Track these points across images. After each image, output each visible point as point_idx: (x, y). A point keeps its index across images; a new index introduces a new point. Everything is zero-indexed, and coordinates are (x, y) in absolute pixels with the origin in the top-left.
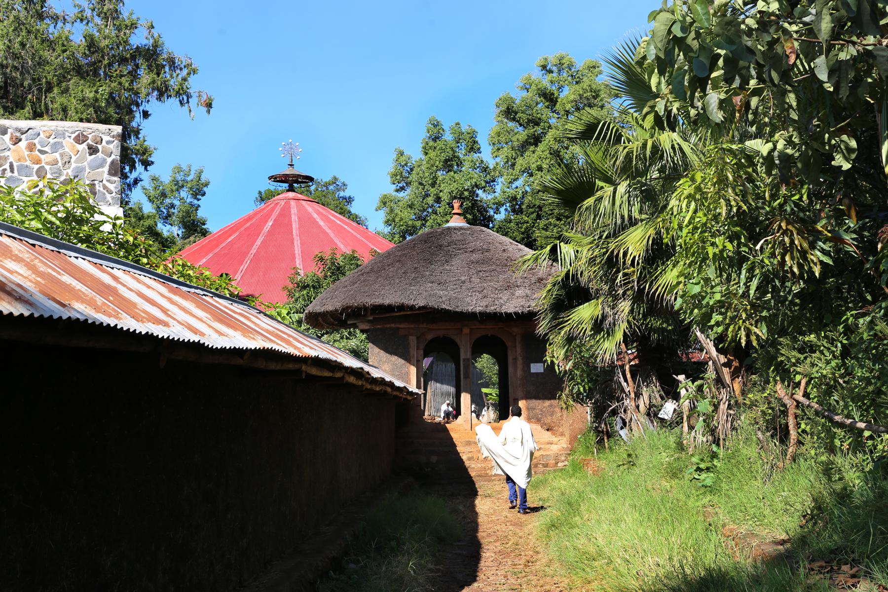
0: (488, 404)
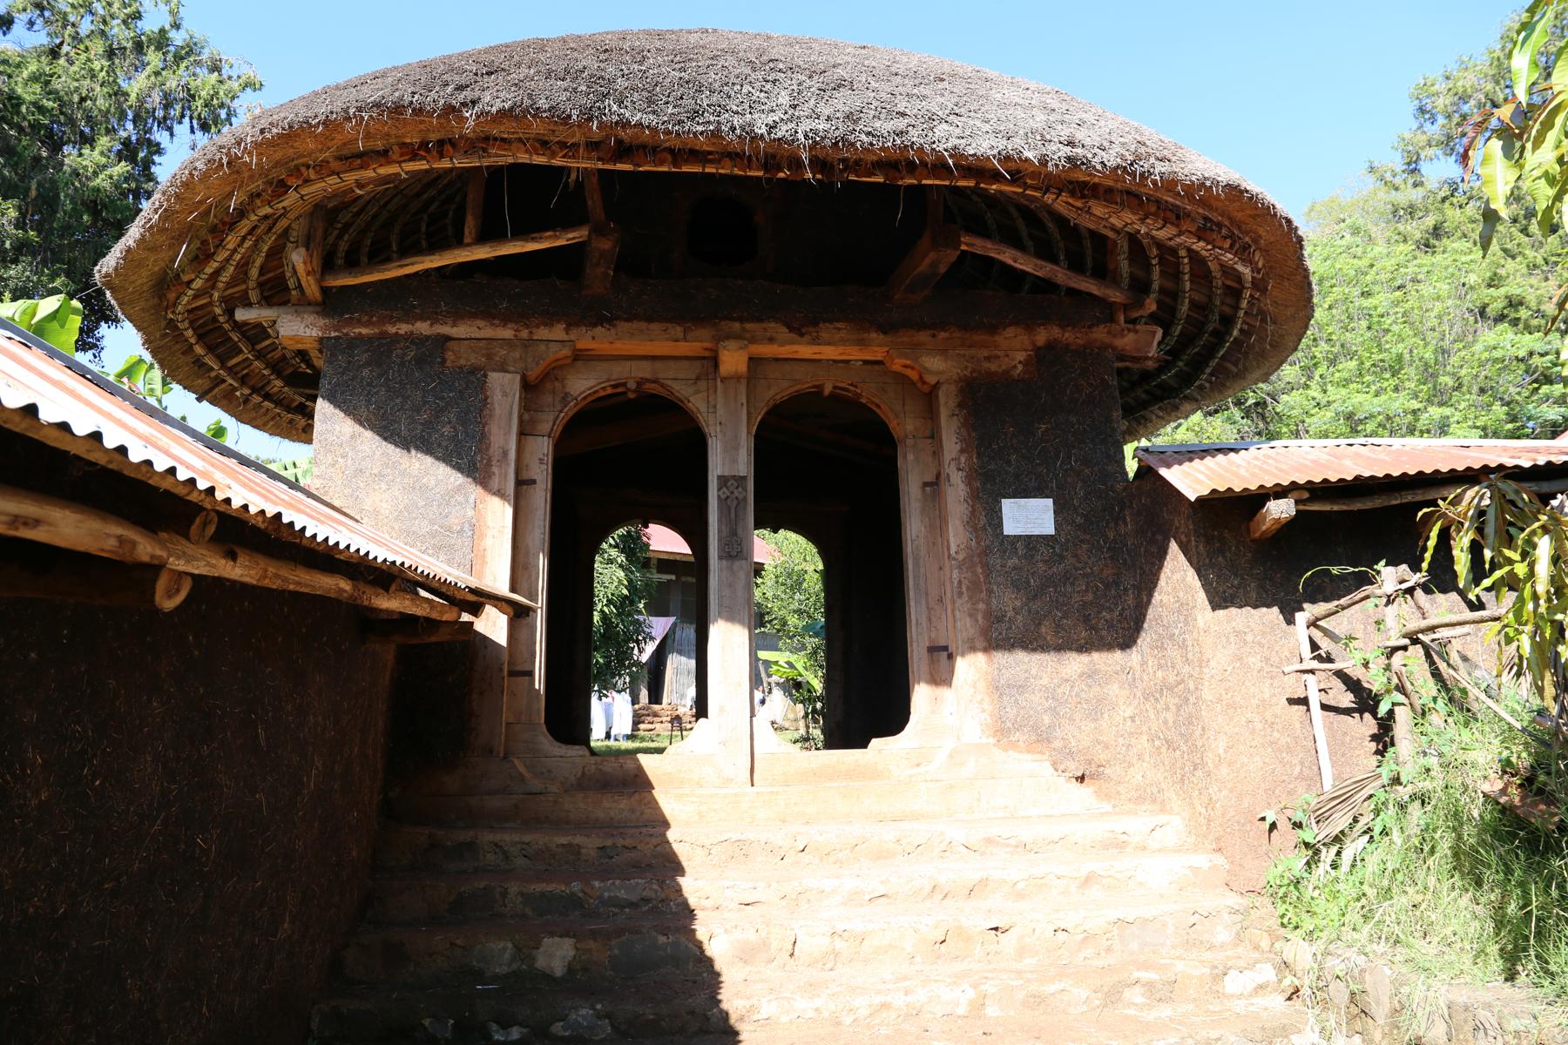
0: (769, 684)
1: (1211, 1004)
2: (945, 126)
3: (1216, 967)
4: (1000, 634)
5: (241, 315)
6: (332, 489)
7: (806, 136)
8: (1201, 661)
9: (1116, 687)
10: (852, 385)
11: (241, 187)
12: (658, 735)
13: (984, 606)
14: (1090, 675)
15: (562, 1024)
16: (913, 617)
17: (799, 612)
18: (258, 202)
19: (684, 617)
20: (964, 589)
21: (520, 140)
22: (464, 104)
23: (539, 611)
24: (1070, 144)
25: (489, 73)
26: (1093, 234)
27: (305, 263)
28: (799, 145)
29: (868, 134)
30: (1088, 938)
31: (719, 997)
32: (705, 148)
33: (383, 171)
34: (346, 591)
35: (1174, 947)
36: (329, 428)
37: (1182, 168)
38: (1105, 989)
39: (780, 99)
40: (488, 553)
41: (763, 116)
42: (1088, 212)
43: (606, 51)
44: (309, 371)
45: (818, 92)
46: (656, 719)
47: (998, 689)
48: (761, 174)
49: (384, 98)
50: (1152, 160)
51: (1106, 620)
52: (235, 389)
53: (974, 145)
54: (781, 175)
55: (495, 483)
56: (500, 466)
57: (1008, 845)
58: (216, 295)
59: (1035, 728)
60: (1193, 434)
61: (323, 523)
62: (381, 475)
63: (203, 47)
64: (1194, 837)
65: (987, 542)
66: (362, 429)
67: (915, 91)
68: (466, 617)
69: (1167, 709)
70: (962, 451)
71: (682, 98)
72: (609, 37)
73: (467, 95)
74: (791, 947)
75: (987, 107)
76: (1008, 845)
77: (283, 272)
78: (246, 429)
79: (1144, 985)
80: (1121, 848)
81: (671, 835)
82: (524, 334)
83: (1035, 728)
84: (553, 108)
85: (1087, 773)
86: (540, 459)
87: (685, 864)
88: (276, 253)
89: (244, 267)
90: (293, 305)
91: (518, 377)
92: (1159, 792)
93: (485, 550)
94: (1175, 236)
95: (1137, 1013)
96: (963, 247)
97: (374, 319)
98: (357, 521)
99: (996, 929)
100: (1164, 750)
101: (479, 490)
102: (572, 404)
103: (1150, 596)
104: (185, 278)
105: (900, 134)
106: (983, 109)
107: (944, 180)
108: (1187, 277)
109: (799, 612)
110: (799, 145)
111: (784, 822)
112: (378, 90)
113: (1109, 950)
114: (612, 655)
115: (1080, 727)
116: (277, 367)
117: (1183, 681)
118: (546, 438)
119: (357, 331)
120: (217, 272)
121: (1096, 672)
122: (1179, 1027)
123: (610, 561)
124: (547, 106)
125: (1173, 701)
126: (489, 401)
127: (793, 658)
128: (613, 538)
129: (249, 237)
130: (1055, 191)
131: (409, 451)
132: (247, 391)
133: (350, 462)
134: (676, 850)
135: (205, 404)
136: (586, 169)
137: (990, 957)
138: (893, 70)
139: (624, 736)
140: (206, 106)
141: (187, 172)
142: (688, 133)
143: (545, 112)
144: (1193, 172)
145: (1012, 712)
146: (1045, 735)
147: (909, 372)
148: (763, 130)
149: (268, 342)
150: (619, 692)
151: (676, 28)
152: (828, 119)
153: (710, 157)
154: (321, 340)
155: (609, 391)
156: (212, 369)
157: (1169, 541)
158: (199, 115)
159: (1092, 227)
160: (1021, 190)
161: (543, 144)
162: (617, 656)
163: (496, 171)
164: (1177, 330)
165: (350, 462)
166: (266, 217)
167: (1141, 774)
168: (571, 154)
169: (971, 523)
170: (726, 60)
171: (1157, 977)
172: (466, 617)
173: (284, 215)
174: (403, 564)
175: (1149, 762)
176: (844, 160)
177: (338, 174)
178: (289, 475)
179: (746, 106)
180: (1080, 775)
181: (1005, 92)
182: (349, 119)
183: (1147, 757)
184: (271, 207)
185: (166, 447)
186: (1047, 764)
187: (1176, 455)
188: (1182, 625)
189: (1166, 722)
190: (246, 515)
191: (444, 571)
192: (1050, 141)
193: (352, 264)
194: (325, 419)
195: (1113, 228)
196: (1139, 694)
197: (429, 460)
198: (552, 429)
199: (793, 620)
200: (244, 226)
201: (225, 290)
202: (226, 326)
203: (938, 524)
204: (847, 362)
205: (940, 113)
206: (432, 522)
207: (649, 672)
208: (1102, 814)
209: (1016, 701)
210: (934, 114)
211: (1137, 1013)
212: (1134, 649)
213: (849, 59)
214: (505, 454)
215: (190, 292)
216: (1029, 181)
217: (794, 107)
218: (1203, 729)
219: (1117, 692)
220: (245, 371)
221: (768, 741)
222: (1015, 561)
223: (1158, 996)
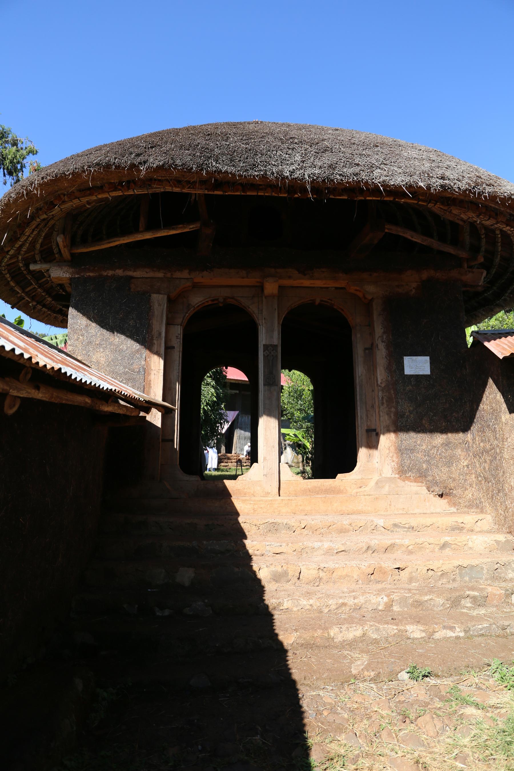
0: (285, 445)
1: (505, 608)
2: (379, 170)
3: (508, 590)
4: (402, 423)
5: (32, 267)
6: (77, 351)
7: (309, 176)
8: (503, 439)
9: (459, 450)
10: (329, 299)
11: (32, 205)
12: (230, 469)
13: (395, 410)
14: (447, 444)
15: (188, 608)
16: (359, 414)
17: (300, 410)
18: (40, 212)
19: (243, 411)
20: (385, 401)
21: (167, 180)
22: (140, 163)
23: (176, 411)
24: (443, 178)
25: (152, 147)
26: (452, 223)
27: (63, 242)
28: (305, 181)
29: (340, 175)
30: (444, 574)
31: (264, 598)
32: (258, 183)
33: (100, 196)
34: (88, 403)
35: (487, 579)
36: (75, 321)
37: (500, 190)
38: (452, 599)
39: (296, 158)
40: (152, 383)
41: (288, 167)
42: (450, 212)
43: (209, 135)
44: (64, 293)
45: (315, 154)
46: (229, 461)
47: (400, 451)
48: (286, 195)
49: (101, 161)
50: (484, 186)
51: (455, 417)
52: (29, 303)
53: (393, 180)
54: (296, 196)
55: (155, 348)
56: (158, 340)
57: (405, 528)
58: (20, 257)
59: (419, 470)
60: (499, 322)
61: (78, 371)
62: (100, 344)
63: (9, 134)
64: (497, 526)
65: (396, 378)
66: (91, 322)
67: (364, 152)
68: (142, 414)
69: (486, 462)
70: (384, 333)
71: (247, 158)
72: (210, 127)
73: (141, 158)
74: (298, 575)
75: (400, 160)
76: (405, 528)
77: (52, 245)
78: (35, 322)
79: (471, 598)
80: (461, 530)
81: (241, 519)
82: (169, 275)
83: (419, 470)
84: (184, 164)
85: (444, 493)
86: (177, 336)
87: (247, 533)
88: (48, 237)
89: (33, 244)
90: (57, 262)
91: (166, 296)
92: (480, 503)
93: (150, 381)
94: (494, 224)
95: (468, 612)
96: (386, 231)
97: (96, 268)
98: (89, 367)
99: (399, 568)
100: (483, 482)
101: (148, 352)
102: (192, 309)
103: (478, 406)
104: (6, 250)
105: (356, 174)
106: (398, 161)
107: (378, 198)
108: (499, 244)
109: (300, 410)
110: (305, 181)
111: (295, 514)
112: (98, 157)
113: (454, 580)
114: (208, 430)
115: (441, 470)
116: (48, 292)
117: (494, 448)
118: (179, 326)
119: (88, 274)
120: (21, 246)
121: (450, 443)
122: (489, 619)
123: (208, 384)
124: (181, 164)
125: (488, 458)
126: (152, 308)
127: (297, 433)
128: (209, 373)
129: (36, 229)
130: (434, 202)
131: (114, 333)
132: (35, 303)
133: (85, 338)
134: (243, 527)
135: (15, 309)
136: (200, 194)
137: (395, 582)
138: (352, 141)
139: (213, 469)
140: (11, 163)
141: (7, 199)
142: (251, 176)
143: (180, 166)
144: (505, 191)
145: (407, 462)
146: (424, 474)
147: (358, 293)
148: (288, 174)
149: (44, 280)
150: (212, 448)
151: (242, 121)
152: (320, 167)
153: (261, 187)
154: (70, 279)
155: (210, 303)
156: (18, 293)
157: (488, 378)
158: (8, 167)
159: (451, 219)
160: (416, 202)
161: (178, 182)
162: (210, 430)
163: (155, 195)
164: (494, 271)
165: (85, 338)
166: (44, 220)
167: (471, 494)
168: (192, 186)
169: (388, 369)
170: (269, 138)
171: (478, 594)
172: (142, 414)
173: (52, 218)
174: (115, 390)
175: (475, 488)
176: (328, 188)
177: (79, 198)
178: (53, 342)
179: (279, 162)
180: (440, 493)
181: (409, 152)
182: (84, 171)
183: (474, 486)
184: (47, 215)
185: (7, 336)
186: (425, 488)
187: (492, 335)
188: (493, 420)
189: (484, 468)
190: (45, 369)
191: (133, 392)
192: (432, 177)
193: (84, 242)
194: (74, 317)
195: (462, 220)
196: (471, 454)
197: (123, 337)
198: (182, 322)
199: (297, 414)
200: (34, 224)
201: (25, 254)
202: (25, 272)
203: (372, 367)
204: (327, 288)
205: (376, 164)
206: (125, 367)
207: (226, 438)
208: (451, 513)
209: (410, 457)
210: (373, 164)
211: (468, 612)
212: (469, 432)
213: (330, 136)
214: (160, 334)
215: (8, 256)
216: (421, 197)
217: (303, 162)
218: (504, 472)
219: (460, 453)
220: (34, 294)
221: (288, 474)
222: (410, 387)
223: (478, 604)
